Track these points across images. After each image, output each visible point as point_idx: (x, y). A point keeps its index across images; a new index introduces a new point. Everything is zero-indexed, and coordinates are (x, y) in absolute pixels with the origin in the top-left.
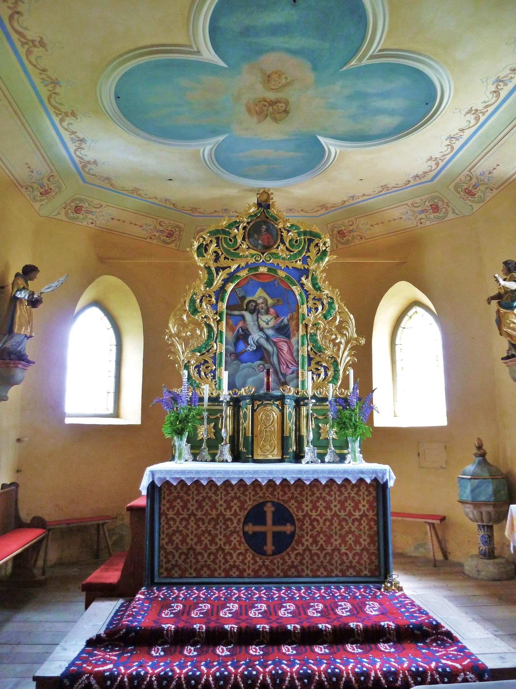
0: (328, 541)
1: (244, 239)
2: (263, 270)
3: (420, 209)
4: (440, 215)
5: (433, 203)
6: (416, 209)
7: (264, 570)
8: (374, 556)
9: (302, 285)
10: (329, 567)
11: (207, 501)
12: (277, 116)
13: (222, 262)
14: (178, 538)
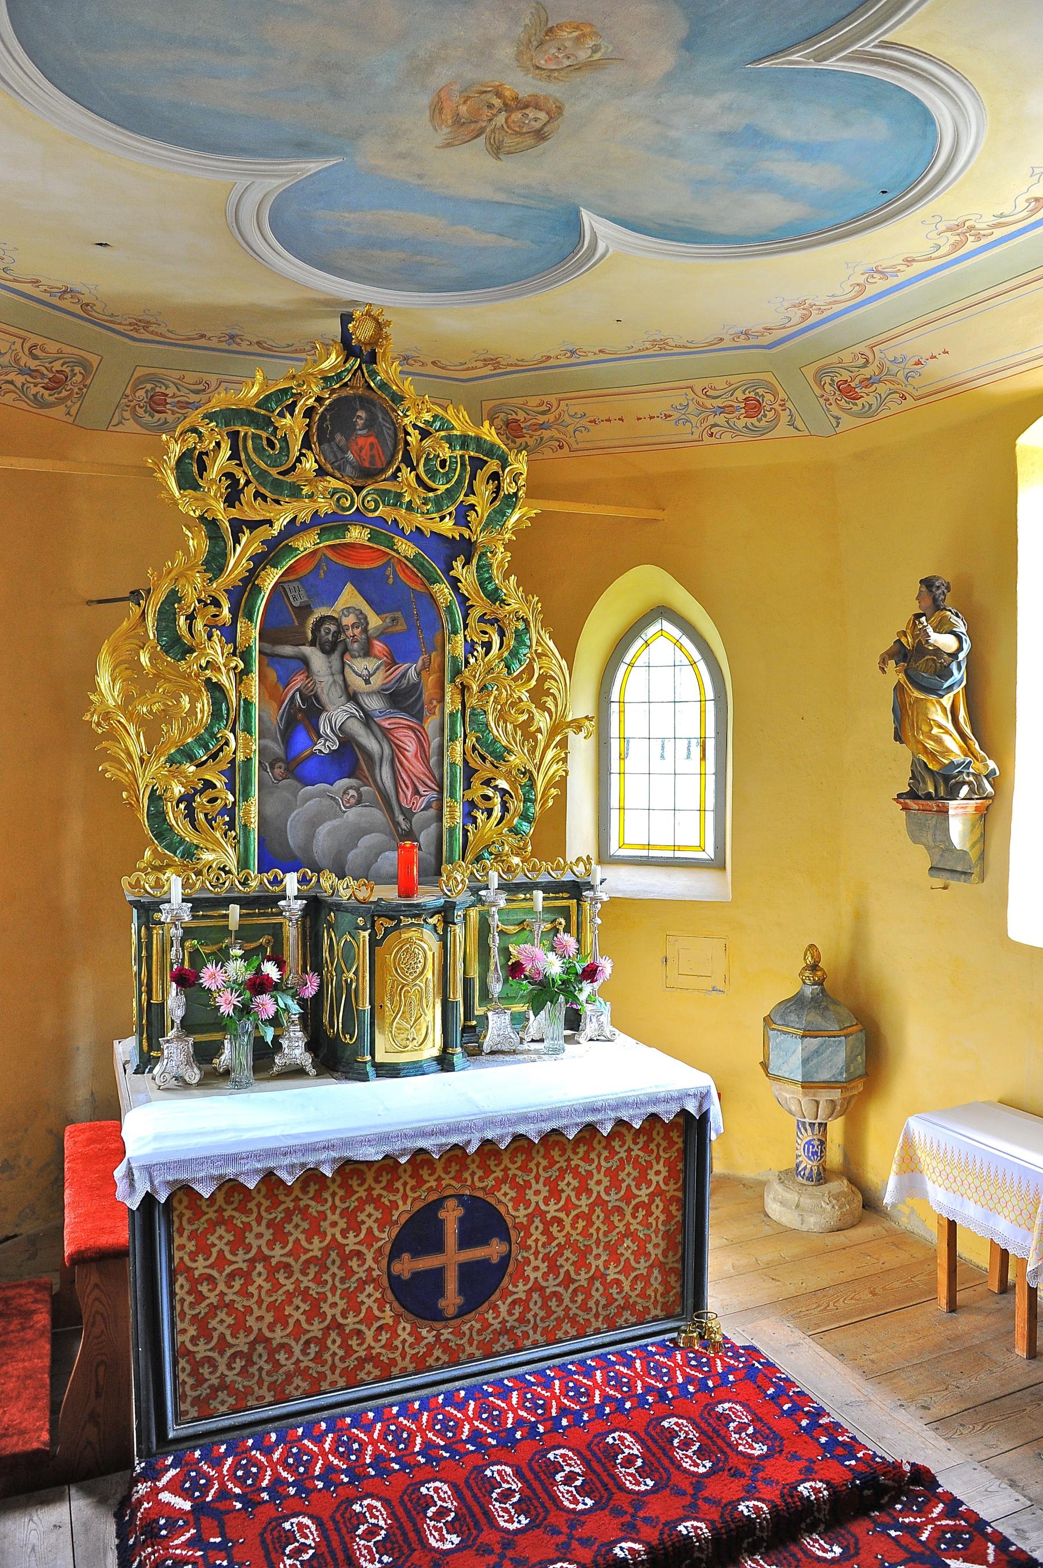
0: (581, 1263)
1: (306, 443)
2: (357, 535)
3: (719, 402)
4: (757, 424)
5: (752, 395)
6: (709, 403)
7: (437, 1352)
8: (673, 1275)
9: (454, 582)
10: (582, 1317)
11: (297, 1219)
12: (509, 141)
13: (250, 509)
14: (221, 1324)
